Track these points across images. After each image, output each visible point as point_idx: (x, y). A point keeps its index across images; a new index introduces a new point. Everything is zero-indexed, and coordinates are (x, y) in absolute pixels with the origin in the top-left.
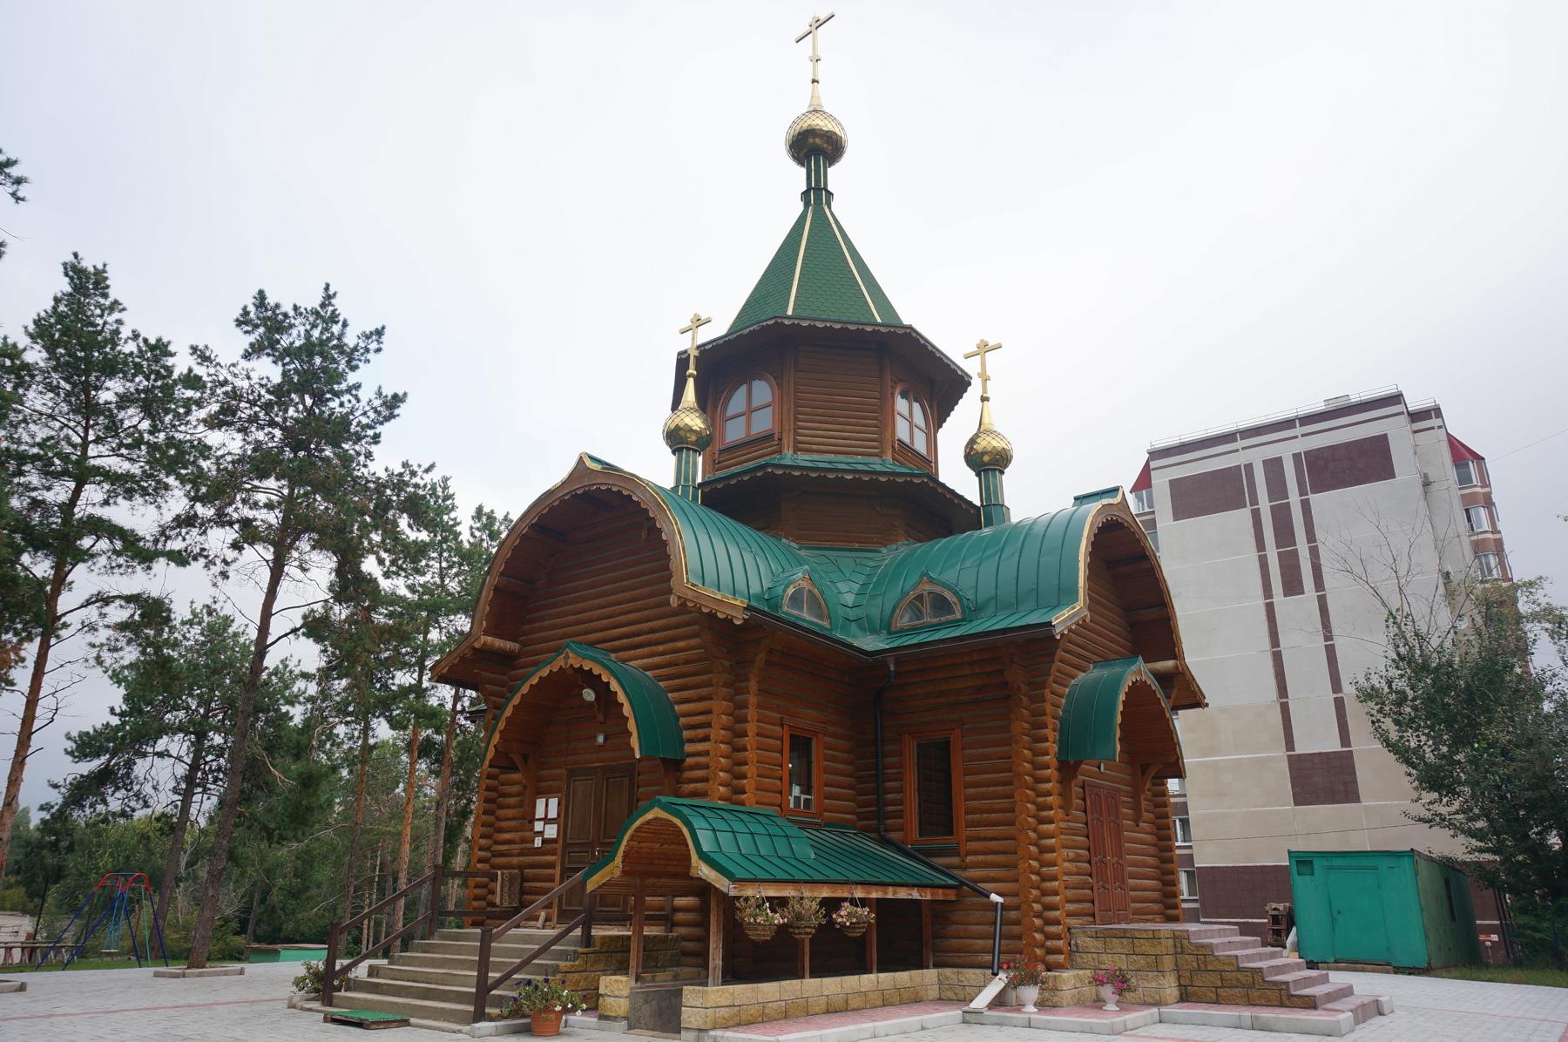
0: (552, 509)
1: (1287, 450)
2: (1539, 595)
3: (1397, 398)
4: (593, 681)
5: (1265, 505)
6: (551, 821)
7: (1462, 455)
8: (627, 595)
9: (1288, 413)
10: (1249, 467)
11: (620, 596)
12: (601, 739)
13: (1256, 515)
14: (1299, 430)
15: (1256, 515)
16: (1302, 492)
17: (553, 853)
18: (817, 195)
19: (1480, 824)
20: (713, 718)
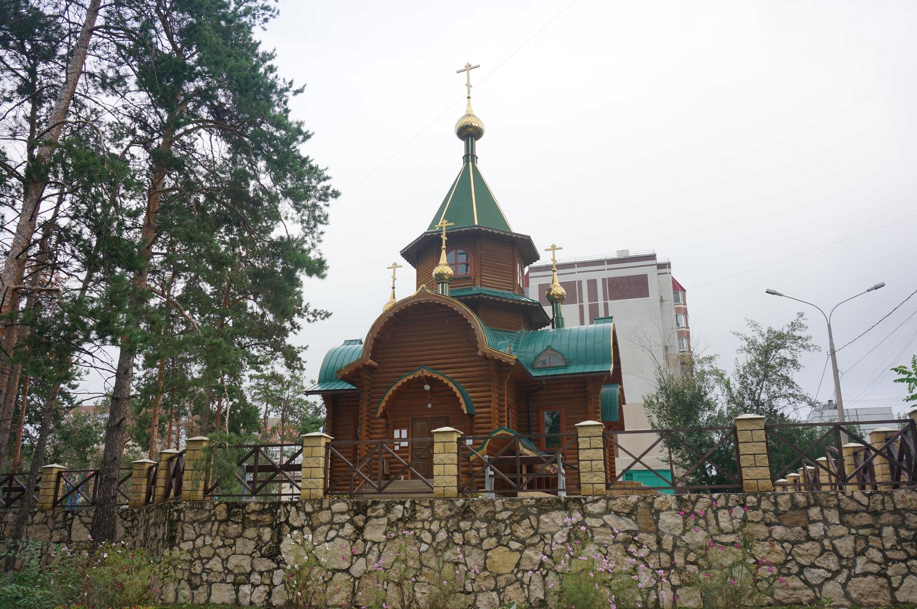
0: (407, 307)
1: (600, 276)
2: (713, 363)
3: (652, 257)
4: (421, 381)
5: (586, 303)
6: (404, 440)
7: (677, 288)
8: (440, 347)
9: (602, 257)
10: (580, 282)
11: (435, 347)
12: (430, 406)
13: (581, 308)
14: (606, 266)
15: (581, 308)
16: (605, 299)
17: (407, 452)
18: (470, 156)
19: (688, 462)
20: (492, 399)
